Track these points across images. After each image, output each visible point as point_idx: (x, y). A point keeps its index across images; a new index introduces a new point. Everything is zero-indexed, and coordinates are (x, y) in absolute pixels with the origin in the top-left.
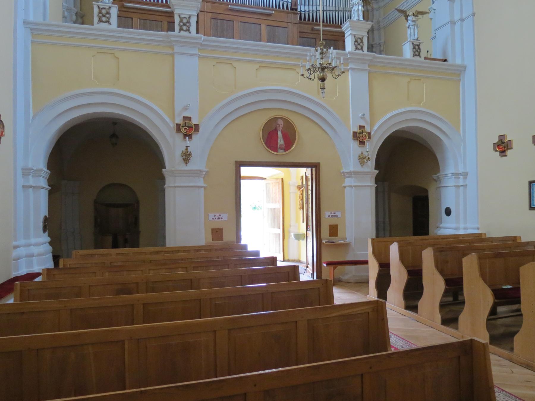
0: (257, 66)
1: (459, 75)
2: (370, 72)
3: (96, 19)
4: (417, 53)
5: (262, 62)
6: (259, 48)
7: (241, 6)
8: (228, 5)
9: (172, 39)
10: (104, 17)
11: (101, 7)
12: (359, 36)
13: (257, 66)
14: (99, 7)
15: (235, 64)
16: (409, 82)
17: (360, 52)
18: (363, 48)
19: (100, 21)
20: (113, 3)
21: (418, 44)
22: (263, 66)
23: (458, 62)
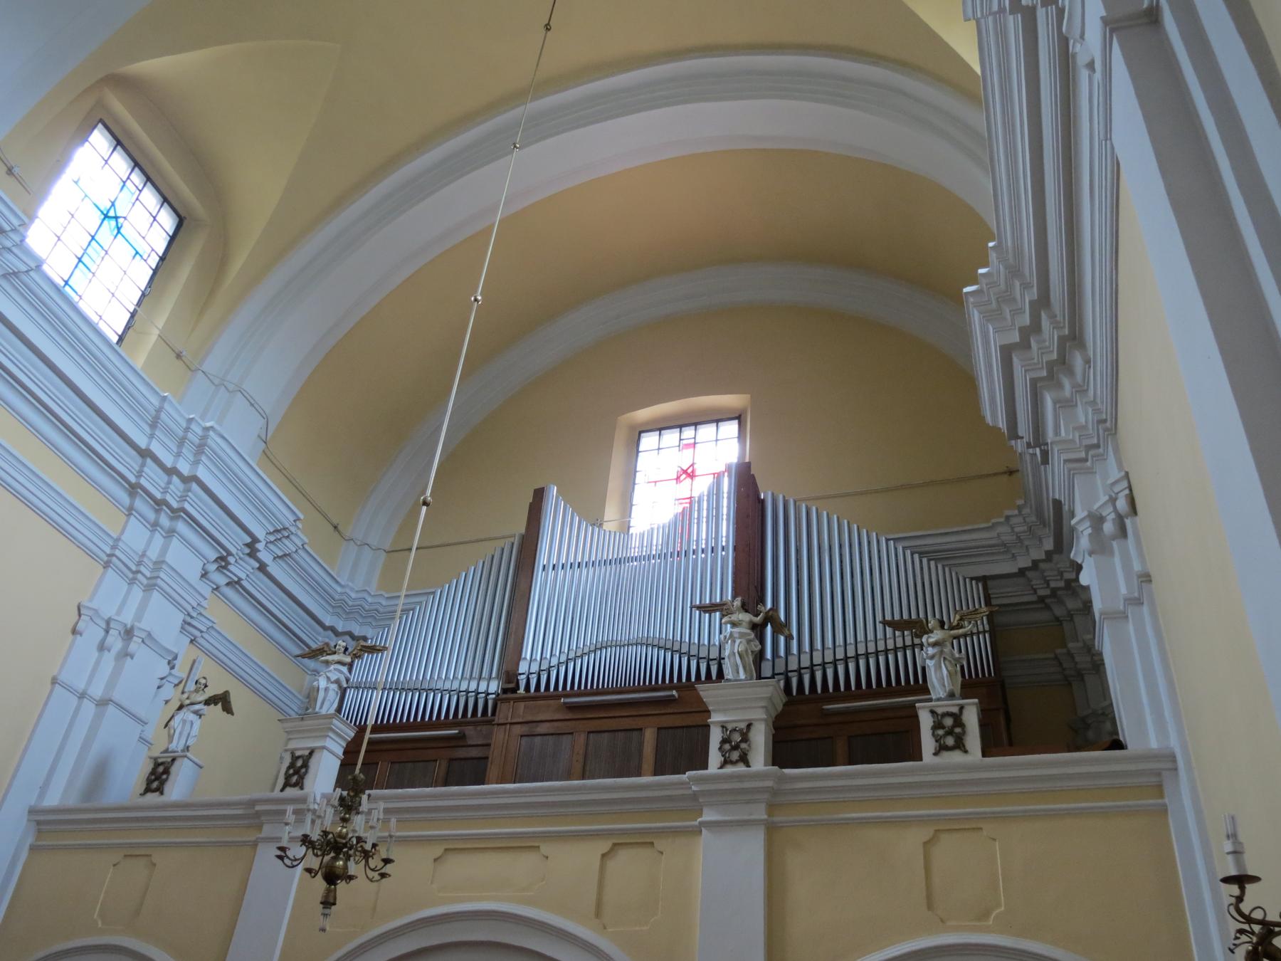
0: (438, 850)
1: (1159, 790)
2: (771, 830)
3: (928, 743)
4: (950, 741)
5: (131, 846)
6: (1034, 772)
7: (598, 693)
8: (559, 697)
9: (258, 808)
10: (951, 735)
11: (940, 711)
12: (734, 725)
13: (438, 850)
14: (933, 712)
15: (545, 848)
16: (927, 844)
17: (741, 768)
18: (751, 757)
19: (941, 748)
20: (964, 696)
21: (955, 710)
22: (455, 847)
23: (1154, 744)
